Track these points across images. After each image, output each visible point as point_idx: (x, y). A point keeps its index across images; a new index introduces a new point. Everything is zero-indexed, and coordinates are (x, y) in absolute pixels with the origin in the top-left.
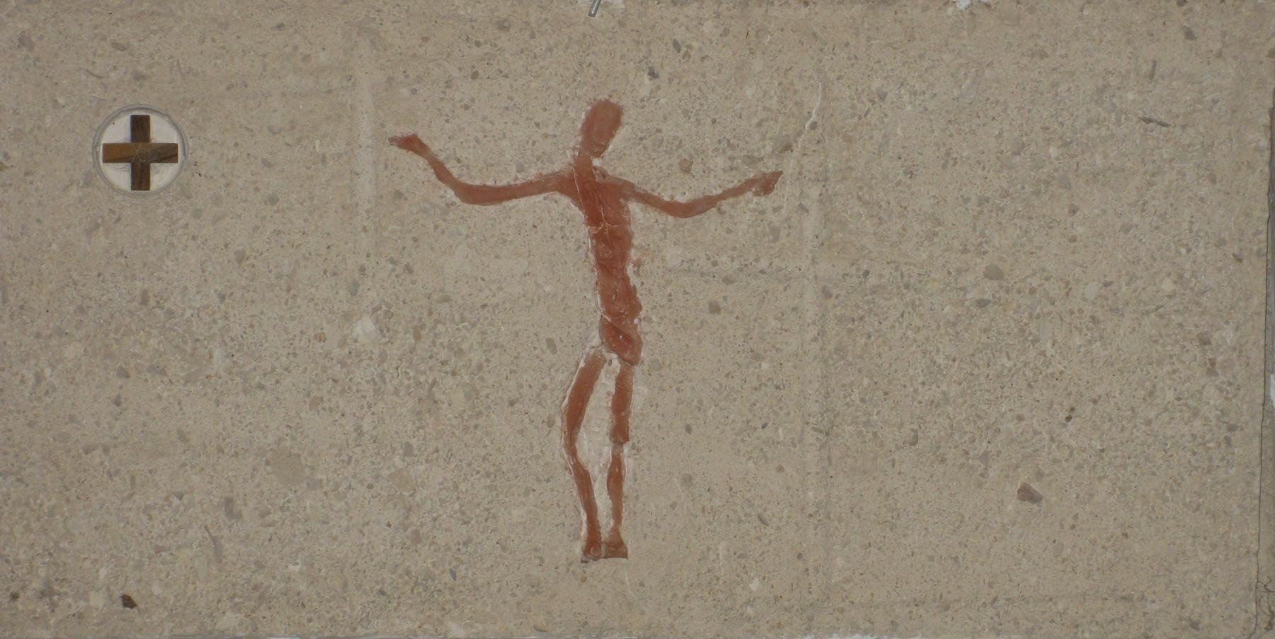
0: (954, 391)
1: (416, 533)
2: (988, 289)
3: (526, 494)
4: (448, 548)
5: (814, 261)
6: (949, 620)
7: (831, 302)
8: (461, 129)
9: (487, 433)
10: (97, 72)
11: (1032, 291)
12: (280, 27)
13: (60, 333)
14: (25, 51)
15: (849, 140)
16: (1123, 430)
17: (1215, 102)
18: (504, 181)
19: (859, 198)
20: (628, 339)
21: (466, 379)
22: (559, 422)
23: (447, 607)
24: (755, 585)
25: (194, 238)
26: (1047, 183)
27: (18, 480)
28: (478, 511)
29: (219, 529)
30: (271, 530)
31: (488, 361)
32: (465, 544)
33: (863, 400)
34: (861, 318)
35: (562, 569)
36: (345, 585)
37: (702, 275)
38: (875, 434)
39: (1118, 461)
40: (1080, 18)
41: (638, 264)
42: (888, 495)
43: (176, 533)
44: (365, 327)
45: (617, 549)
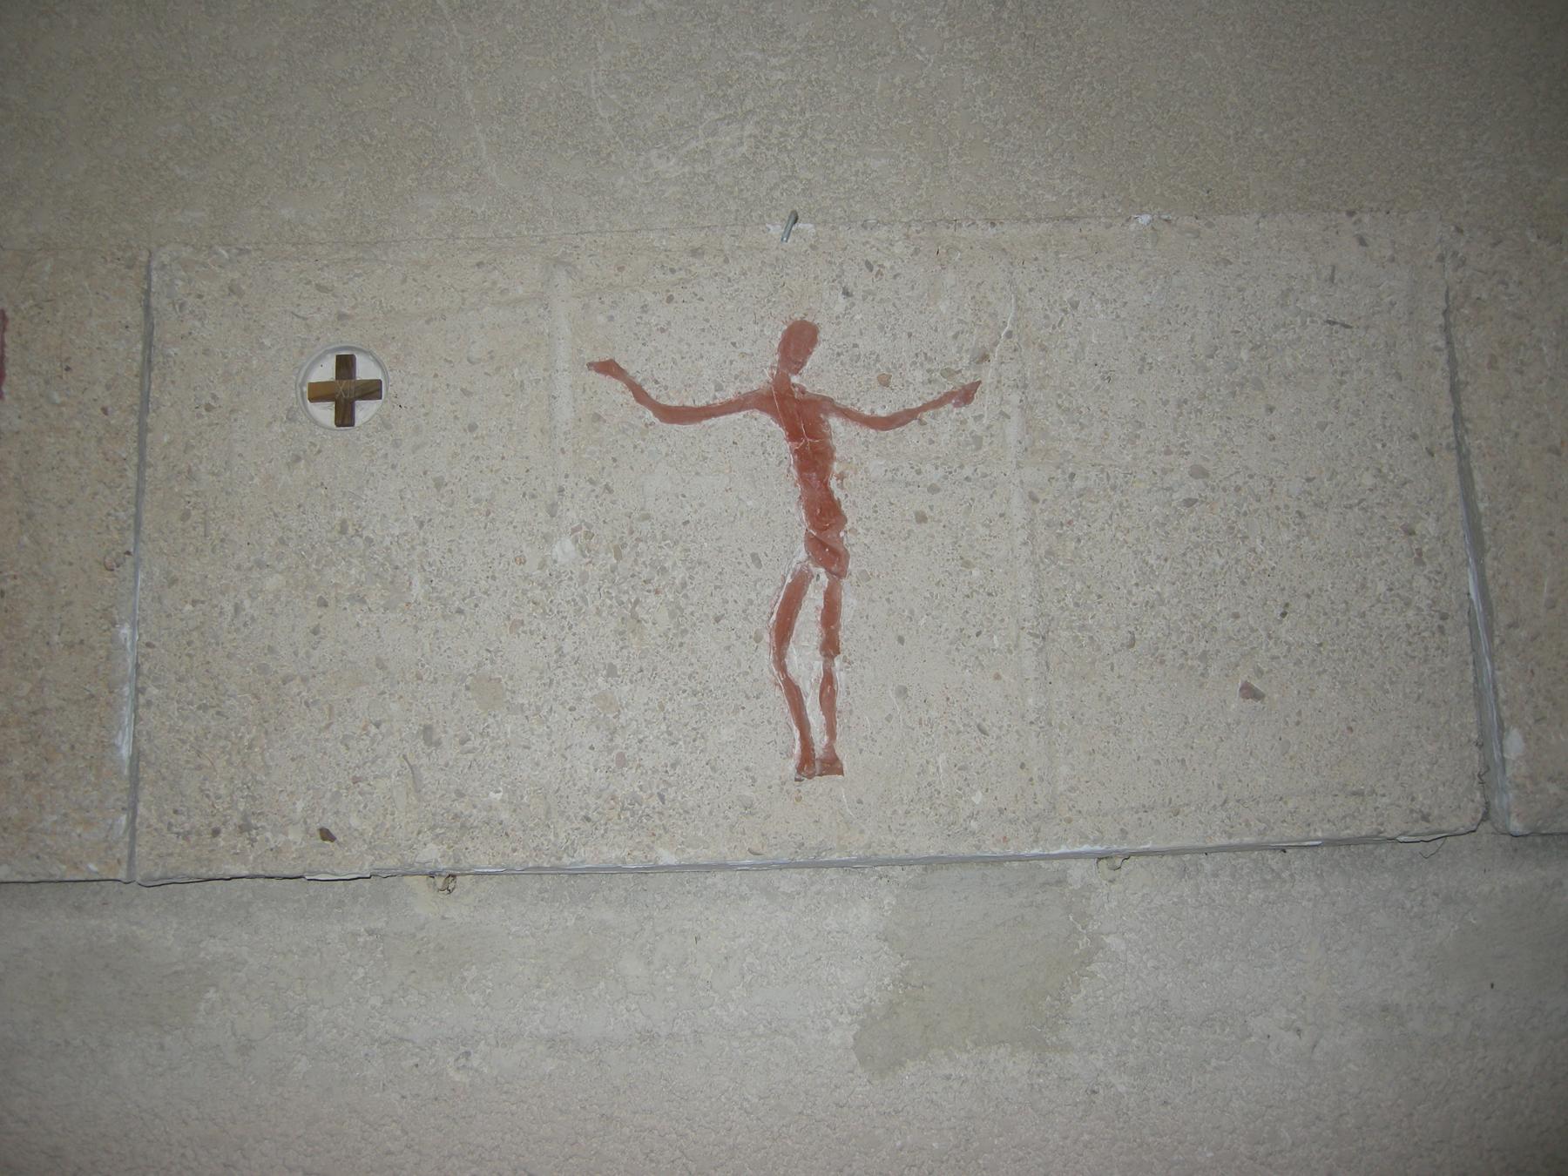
0: (1168, 591)
1: (621, 755)
2: (1195, 487)
3: (736, 711)
4: (655, 771)
5: (1019, 466)
6: (1179, 825)
7: (1037, 507)
8: (658, 351)
9: (693, 651)
10: (302, 314)
11: (1238, 489)
12: (479, 265)
13: (260, 564)
14: (235, 298)
15: (1044, 349)
16: (1337, 623)
17: (1392, 304)
18: (701, 403)
19: (1059, 406)
20: (834, 552)
21: (670, 597)
22: (766, 638)
23: (657, 832)
24: (978, 798)
25: (394, 467)
26: (1242, 385)
27: (218, 713)
28: (685, 731)
29: (418, 757)
30: (471, 756)
31: (691, 578)
32: (674, 766)
33: (1077, 605)
34: (1070, 523)
35: (775, 789)
36: (548, 812)
37: (908, 484)
38: (1091, 638)
39: (1336, 656)
40: (1258, 230)
41: (841, 477)
42: (1109, 699)
43: (373, 762)
44: (564, 550)
45: (832, 765)
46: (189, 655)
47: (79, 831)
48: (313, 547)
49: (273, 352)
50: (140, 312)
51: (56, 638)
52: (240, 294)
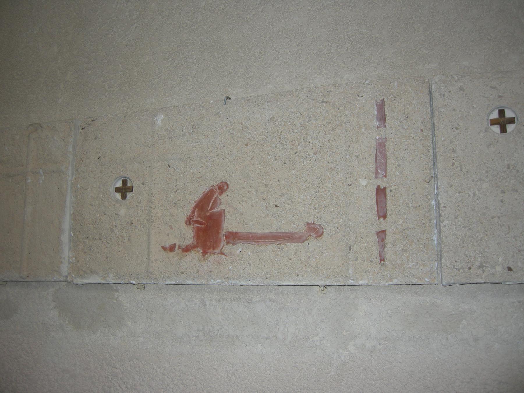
14: (462, 92)
27: (469, 229)
46: (458, 210)
47: (421, 268)
48: (498, 173)
49: (477, 109)
50: (429, 97)
51: (411, 205)
52: (464, 91)
